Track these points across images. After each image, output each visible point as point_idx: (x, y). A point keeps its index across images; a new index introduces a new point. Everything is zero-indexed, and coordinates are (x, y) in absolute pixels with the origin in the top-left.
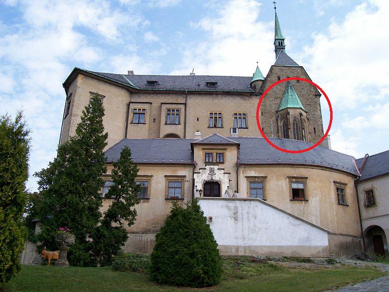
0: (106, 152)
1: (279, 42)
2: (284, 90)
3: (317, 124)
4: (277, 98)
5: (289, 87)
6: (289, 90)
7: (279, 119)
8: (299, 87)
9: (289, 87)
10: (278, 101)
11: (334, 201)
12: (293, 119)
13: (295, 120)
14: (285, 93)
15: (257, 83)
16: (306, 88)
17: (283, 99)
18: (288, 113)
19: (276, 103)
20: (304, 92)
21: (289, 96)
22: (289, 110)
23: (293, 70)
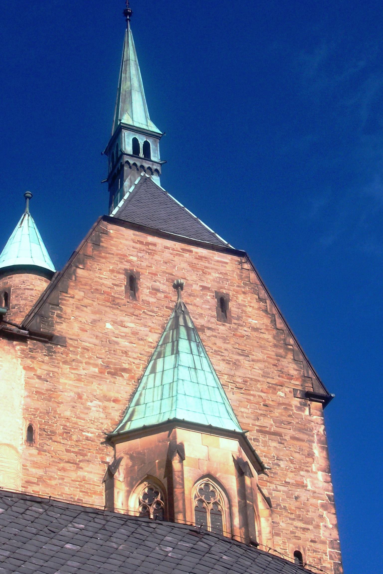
0: (26, 202)
1: (135, 141)
2: (153, 338)
3: (309, 536)
4: (116, 372)
5: (183, 331)
6: (183, 344)
7: (120, 476)
8: (225, 340)
9: (183, 331)
10: (121, 387)
11: (322, 433)
12: (200, 484)
13: (207, 493)
14: (160, 355)
15: (16, 280)
16: (259, 355)
17: (149, 381)
18: (177, 450)
19: (113, 395)
20: (251, 369)
21: (183, 373)
22: (182, 435)
23: (201, 258)
